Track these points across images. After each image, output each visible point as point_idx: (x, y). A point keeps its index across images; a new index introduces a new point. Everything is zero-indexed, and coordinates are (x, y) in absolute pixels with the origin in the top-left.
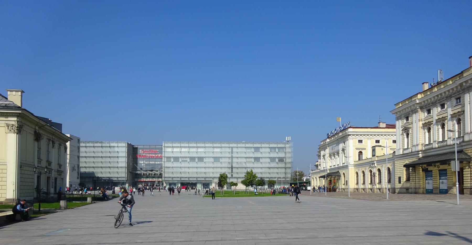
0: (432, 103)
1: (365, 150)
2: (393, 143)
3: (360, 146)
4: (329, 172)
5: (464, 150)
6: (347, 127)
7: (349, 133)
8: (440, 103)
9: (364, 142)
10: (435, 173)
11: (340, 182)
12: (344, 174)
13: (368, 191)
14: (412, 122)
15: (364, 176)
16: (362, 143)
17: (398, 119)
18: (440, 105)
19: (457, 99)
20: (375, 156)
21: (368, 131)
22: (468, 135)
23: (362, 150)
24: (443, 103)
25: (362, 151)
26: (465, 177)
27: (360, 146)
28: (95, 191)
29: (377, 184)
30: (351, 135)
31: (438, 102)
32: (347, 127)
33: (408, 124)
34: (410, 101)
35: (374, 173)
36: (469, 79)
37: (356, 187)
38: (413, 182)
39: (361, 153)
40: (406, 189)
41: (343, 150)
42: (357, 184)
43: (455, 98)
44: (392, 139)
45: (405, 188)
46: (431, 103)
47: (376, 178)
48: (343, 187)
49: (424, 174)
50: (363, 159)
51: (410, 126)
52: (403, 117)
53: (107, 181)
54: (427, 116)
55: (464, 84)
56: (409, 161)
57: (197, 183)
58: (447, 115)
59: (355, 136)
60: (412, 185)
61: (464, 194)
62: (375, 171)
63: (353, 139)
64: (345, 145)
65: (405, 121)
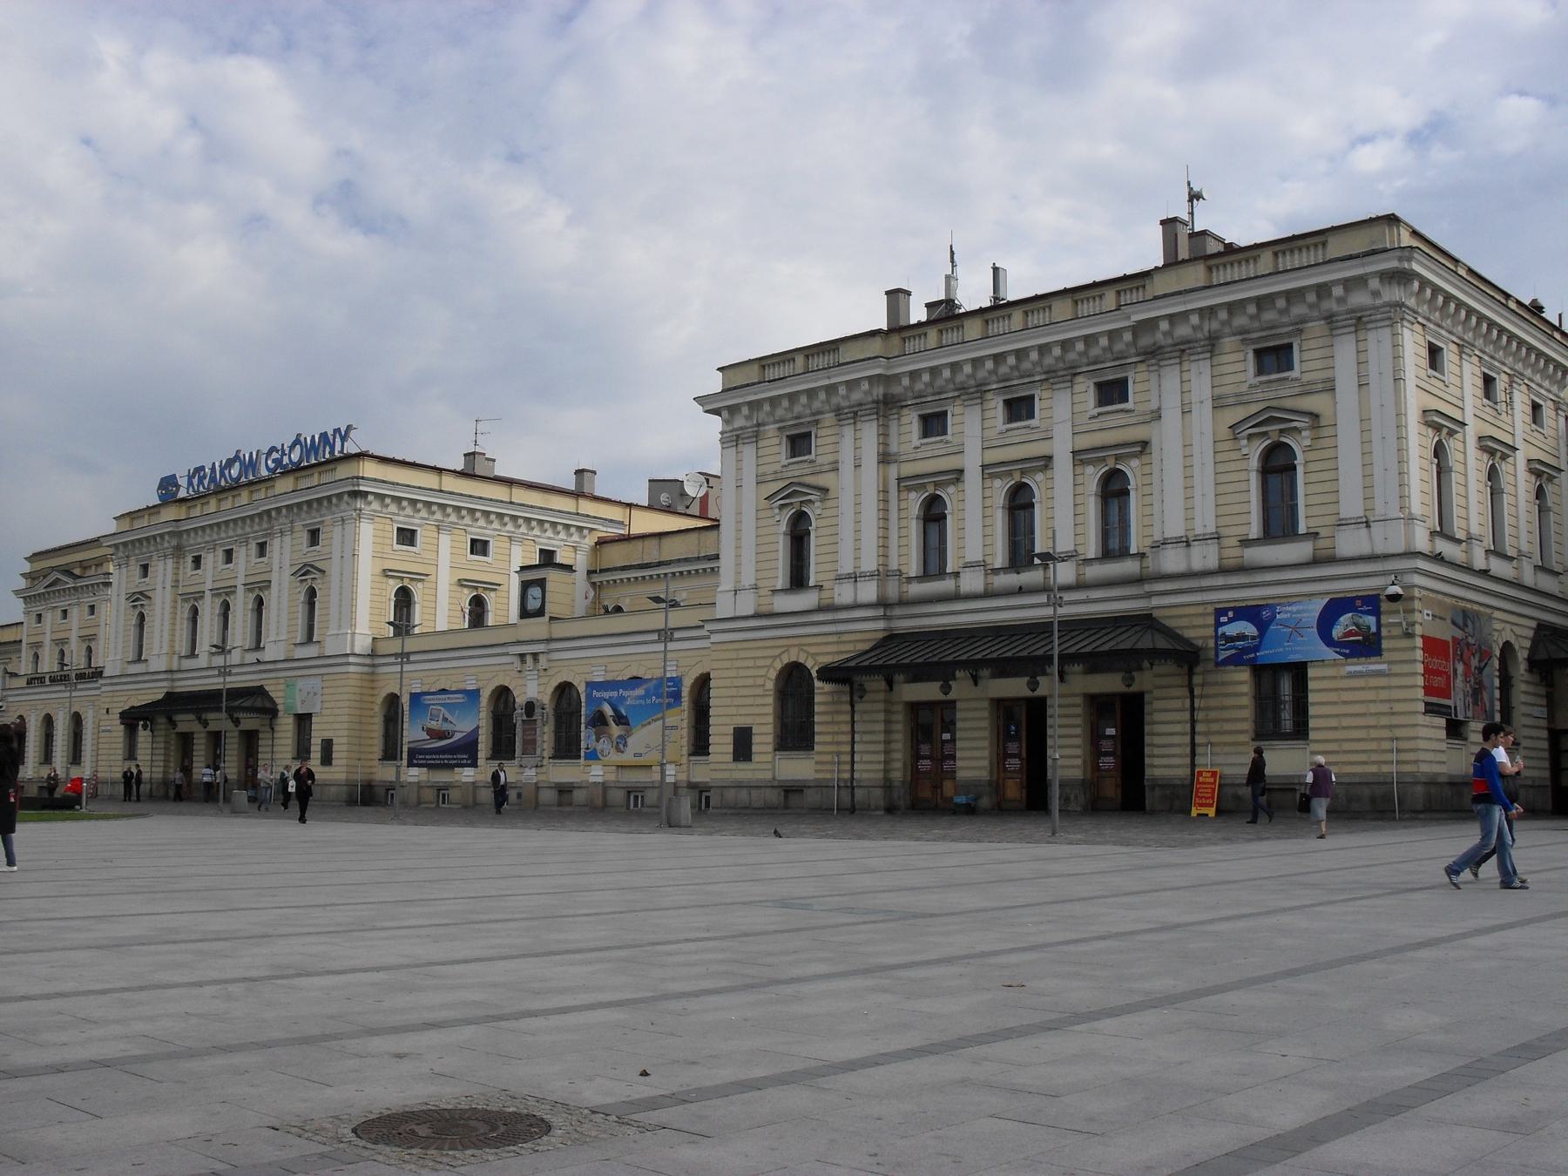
0: (962, 389)
3: (403, 558)
6: (332, 452)
8: (1006, 393)
10: (114, 746)
14: (837, 462)
18: (919, 416)
26: (1316, 707)
27: (403, 558)
30: (367, 493)
32: (332, 452)
36: (986, 356)
39: (404, 599)
40: (560, 791)
43: (920, 413)
46: (1133, 351)
50: (810, 585)
53: (946, 736)
57: (1309, 664)
58: (1075, 440)
59: (1282, 312)
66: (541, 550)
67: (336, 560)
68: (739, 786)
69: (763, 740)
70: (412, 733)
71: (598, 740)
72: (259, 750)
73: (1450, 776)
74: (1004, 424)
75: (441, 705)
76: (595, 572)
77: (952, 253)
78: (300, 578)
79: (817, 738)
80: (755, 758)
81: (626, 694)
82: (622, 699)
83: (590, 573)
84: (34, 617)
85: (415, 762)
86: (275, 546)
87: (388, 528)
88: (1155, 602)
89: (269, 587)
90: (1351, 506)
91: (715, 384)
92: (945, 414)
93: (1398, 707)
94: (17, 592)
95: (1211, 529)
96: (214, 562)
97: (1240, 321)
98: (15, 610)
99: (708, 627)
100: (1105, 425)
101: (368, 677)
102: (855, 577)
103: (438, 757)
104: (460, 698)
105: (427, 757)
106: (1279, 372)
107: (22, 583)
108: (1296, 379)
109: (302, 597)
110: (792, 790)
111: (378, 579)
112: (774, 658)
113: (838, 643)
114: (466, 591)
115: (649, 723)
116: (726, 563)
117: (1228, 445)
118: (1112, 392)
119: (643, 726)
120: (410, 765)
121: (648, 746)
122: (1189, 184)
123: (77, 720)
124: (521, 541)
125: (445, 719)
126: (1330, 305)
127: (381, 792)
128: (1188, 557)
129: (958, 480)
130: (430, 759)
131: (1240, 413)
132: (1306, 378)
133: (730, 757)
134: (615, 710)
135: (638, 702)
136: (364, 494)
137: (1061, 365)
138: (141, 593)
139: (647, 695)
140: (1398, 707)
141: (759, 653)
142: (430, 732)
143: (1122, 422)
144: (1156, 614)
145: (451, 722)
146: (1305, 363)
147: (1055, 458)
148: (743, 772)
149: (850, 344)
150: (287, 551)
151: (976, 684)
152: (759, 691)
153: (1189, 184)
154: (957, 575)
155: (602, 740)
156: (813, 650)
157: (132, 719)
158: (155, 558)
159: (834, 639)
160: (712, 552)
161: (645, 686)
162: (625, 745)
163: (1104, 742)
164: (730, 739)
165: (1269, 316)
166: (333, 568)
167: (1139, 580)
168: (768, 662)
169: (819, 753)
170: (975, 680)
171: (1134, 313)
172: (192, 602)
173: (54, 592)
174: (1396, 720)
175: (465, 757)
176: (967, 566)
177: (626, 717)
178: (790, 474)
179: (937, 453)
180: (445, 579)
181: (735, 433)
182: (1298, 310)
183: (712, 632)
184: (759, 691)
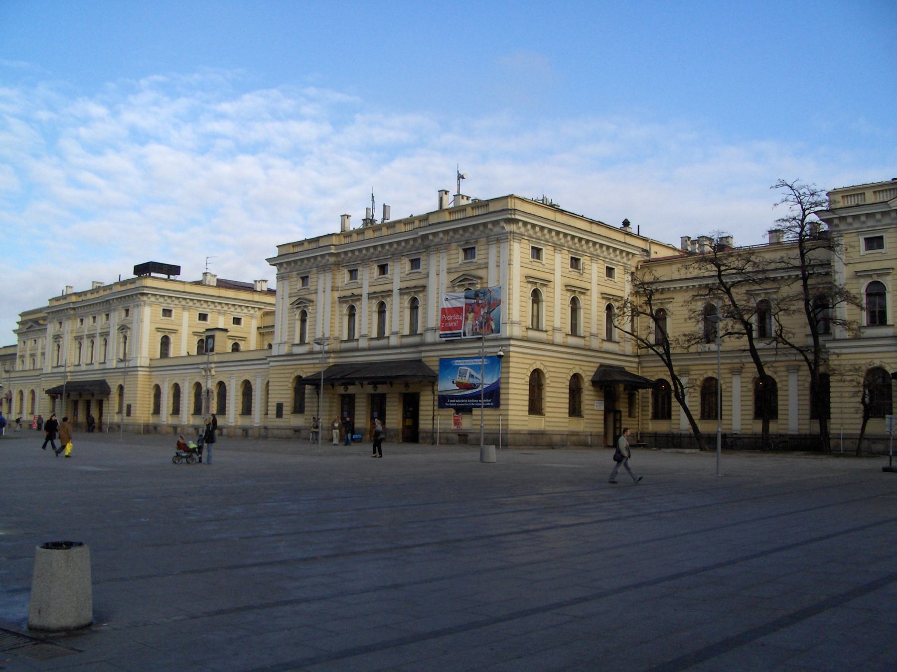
1: (175, 333)
2: (199, 319)
4: (69, 380)
7: (145, 288)
8: (378, 263)
9: (175, 316)
13: (25, 425)
14: (317, 289)
16: (170, 316)
18: (378, 266)
19: (412, 261)
21: (254, 300)
23: (169, 332)
25: (169, 335)
27: (166, 323)
31: (374, 259)
35: (208, 391)
36: (501, 219)
37: (152, 420)
41: (123, 328)
42: (157, 411)
44: (199, 311)
45: (455, 433)
47: (211, 402)
48: (116, 419)
51: (312, 297)
52: (294, 276)
55: (431, 237)
62: (209, 386)
63: (150, 305)
65: (299, 284)
66: (234, 318)
67: (135, 323)
68: (278, 428)
69: (287, 409)
73: (529, 431)
74: (380, 275)
76: (261, 328)
77: (373, 197)
78: (459, 284)
79: (306, 409)
80: (284, 416)
83: (259, 328)
84: (22, 343)
86: (112, 315)
87: (527, 246)
88: (423, 354)
89: (109, 335)
91: (275, 254)
92: (419, 259)
94: (15, 331)
96: (439, 266)
97: (457, 236)
98: (14, 340)
99: (269, 359)
101: (148, 377)
103: (466, 401)
105: (469, 401)
106: (416, 269)
107: (17, 327)
108: (476, 262)
109: (298, 317)
110: (297, 430)
111: (290, 311)
112: (292, 373)
113: (313, 368)
114: (196, 337)
116: (277, 330)
117: (450, 290)
118: (415, 263)
122: (458, 172)
123: (33, 392)
124: (224, 313)
125: (472, 376)
126: (426, 243)
127: (151, 428)
129: (423, 290)
130: (460, 403)
131: (456, 276)
133: (275, 416)
136: (147, 294)
137: (405, 250)
138: (58, 335)
141: (286, 371)
144: (423, 360)
145: (477, 378)
146: (479, 257)
148: (279, 422)
149: (323, 238)
150: (117, 317)
152: (286, 388)
153: (458, 172)
154: (388, 337)
156: (305, 370)
157: (54, 394)
158: (64, 319)
159: (312, 366)
160: (273, 324)
164: (275, 408)
165: (467, 235)
166: (134, 326)
167: (416, 345)
169: (306, 415)
170: (362, 385)
171: (420, 232)
172: (380, 299)
173: (30, 331)
175: (490, 401)
176: (393, 333)
179: (354, 287)
180: (558, 281)
181: (496, 237)
182: (477, 233)
183: (270, 361)
184: (286, 388)
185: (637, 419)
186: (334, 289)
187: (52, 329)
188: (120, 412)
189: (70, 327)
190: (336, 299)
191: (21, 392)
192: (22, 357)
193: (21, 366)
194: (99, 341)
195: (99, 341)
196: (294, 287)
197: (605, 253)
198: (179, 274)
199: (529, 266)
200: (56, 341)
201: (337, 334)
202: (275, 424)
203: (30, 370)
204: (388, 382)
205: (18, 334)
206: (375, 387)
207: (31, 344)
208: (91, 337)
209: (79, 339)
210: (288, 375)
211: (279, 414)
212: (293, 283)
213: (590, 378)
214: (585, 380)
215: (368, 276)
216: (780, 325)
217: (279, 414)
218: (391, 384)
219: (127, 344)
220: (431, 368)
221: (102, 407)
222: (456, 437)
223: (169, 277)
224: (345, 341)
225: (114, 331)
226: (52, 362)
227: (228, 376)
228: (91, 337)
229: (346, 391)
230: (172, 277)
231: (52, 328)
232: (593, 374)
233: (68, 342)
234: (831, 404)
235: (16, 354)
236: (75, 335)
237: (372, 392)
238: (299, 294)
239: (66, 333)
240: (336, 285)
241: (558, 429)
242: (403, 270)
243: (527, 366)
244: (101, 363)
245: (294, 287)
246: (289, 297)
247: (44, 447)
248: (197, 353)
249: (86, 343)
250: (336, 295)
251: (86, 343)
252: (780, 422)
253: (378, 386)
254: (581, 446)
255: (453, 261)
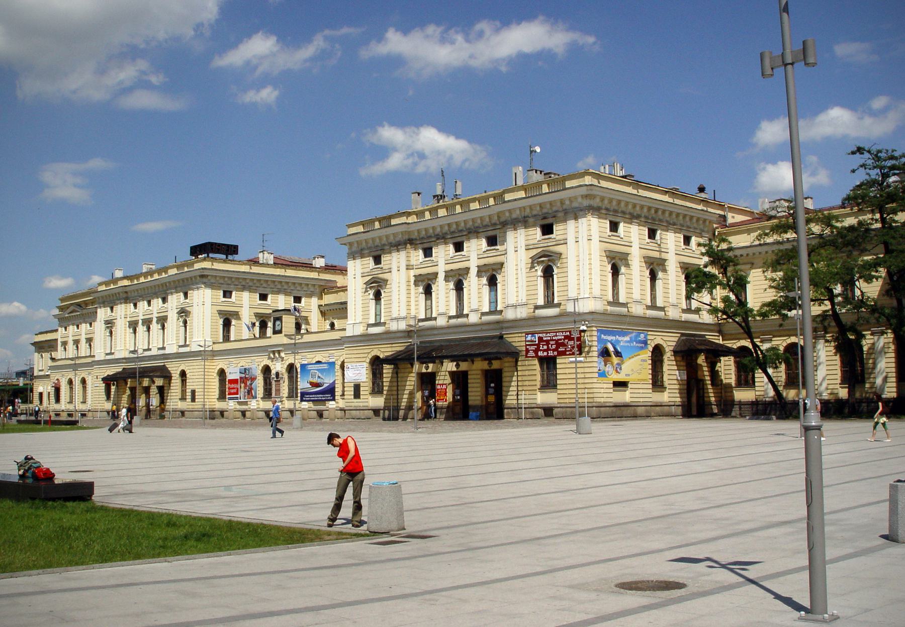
5: (504, 336)
11: (675, 377)
12: (183, 374)
15: (84, 388)
17: (353, 255)
20: (280, 332)
22: (600, 302)
24: (459, 240)
28: (680, 407)
29: (284, 399)
30: (208, 276)
33: (554, 243)
34: (385, 223)
38: (392, 395)
48: (181, 405)
49: (880, 359)
54: (487, 251)
56: (113, 370)
60: (390, 403)
61: (504, 419)
64: (113, 314)
69: (365, 390)
70: (303, 384)
71: (605, 365)
72: (558, 367)
75: (317, 370)
81: (620, 339)
82: (618, 342)
85: (304, 399)
89: (167, 319)
90: (572, 294)
93: (588, 375)
95: (524, 301)
100: (489, 255)
102: (397, 319)
104: (325, 366)
110: (376, 412)
115: (633, 357)
119: (630, 358)
120: (302, 400)
121: (632, 370)
125: (319, 377)
128: (516, 312)
131: (535, 252)
132: (558, 238)
134: (614, 348)
135: (626, 344)
139: (631, 341)
140: (588, 375)
142: (311, 383)
143: (495, 254)
147: (471, 269)
148: (357, 403)
151: (473, 363)
155: (608, 366)
156: (382, 350)
161: (630, 336)
162: (621, 369)
163: (490, 389)
168: (366, 355)
174: (587, 381)
177: (620, 353)
178: (374, 273)
185: (720, 387)
186: (409, 267)
187: (103, 314)
188: (183, 398)
189: (123, 312)
190: (412, 279)
191: (70, 382)
192: (65, 344)
193: (75, 352)
194: (155, 327)
195: (155, 327)
196: (366, 266)
197: (701, 227)
198: (237, 254)
199: (607, 240)
200: (108, 327)
201: (413, 313)
202: (353, 404)
203: (86, 357)
204: (469, 360)
205: (59, 319)
206: (490, 364)
207: (86, 328)
208: (147, 323)
209: (133, 325)
210: (364, 355)
211: (357, 395)
212: (365, 263)
213: (672, 348)
214: (667, 349)
215: (476, 248)
216: (861, 292)
217: (357, 395)
218: (473, 362)
219: (188, 327)
220: (514, 344)
221: (164, 393)
222: (541, 411)
223: (227, 258)
224: (423, 320)
225: (173, 316)
226: (105, 349)
227: (228, 363)
228: (147, 323)
229: (427, 370)
230: (230, 257)
231: (103, 313)
232: (674, 344)
233: (121, 326)
234: (651, 378)
235: (56, 340)
236: (129, 319)
237: (454, 369)
238: (372, 273)
239: (118, 318)
240: (412, 263)
241: (641, 400)
242: (447, 253)
243: (366, 355)
244: (159, 349)
245: (366, 266)
246: (362, 277)
247: (274, 436)
248: (223, 340)
249: (141, 329)
250: (412, 273)
251: (141, 329)
252: (757, 388)
253: (493, 362)
254: (666, 416)
255: (530, 237)
